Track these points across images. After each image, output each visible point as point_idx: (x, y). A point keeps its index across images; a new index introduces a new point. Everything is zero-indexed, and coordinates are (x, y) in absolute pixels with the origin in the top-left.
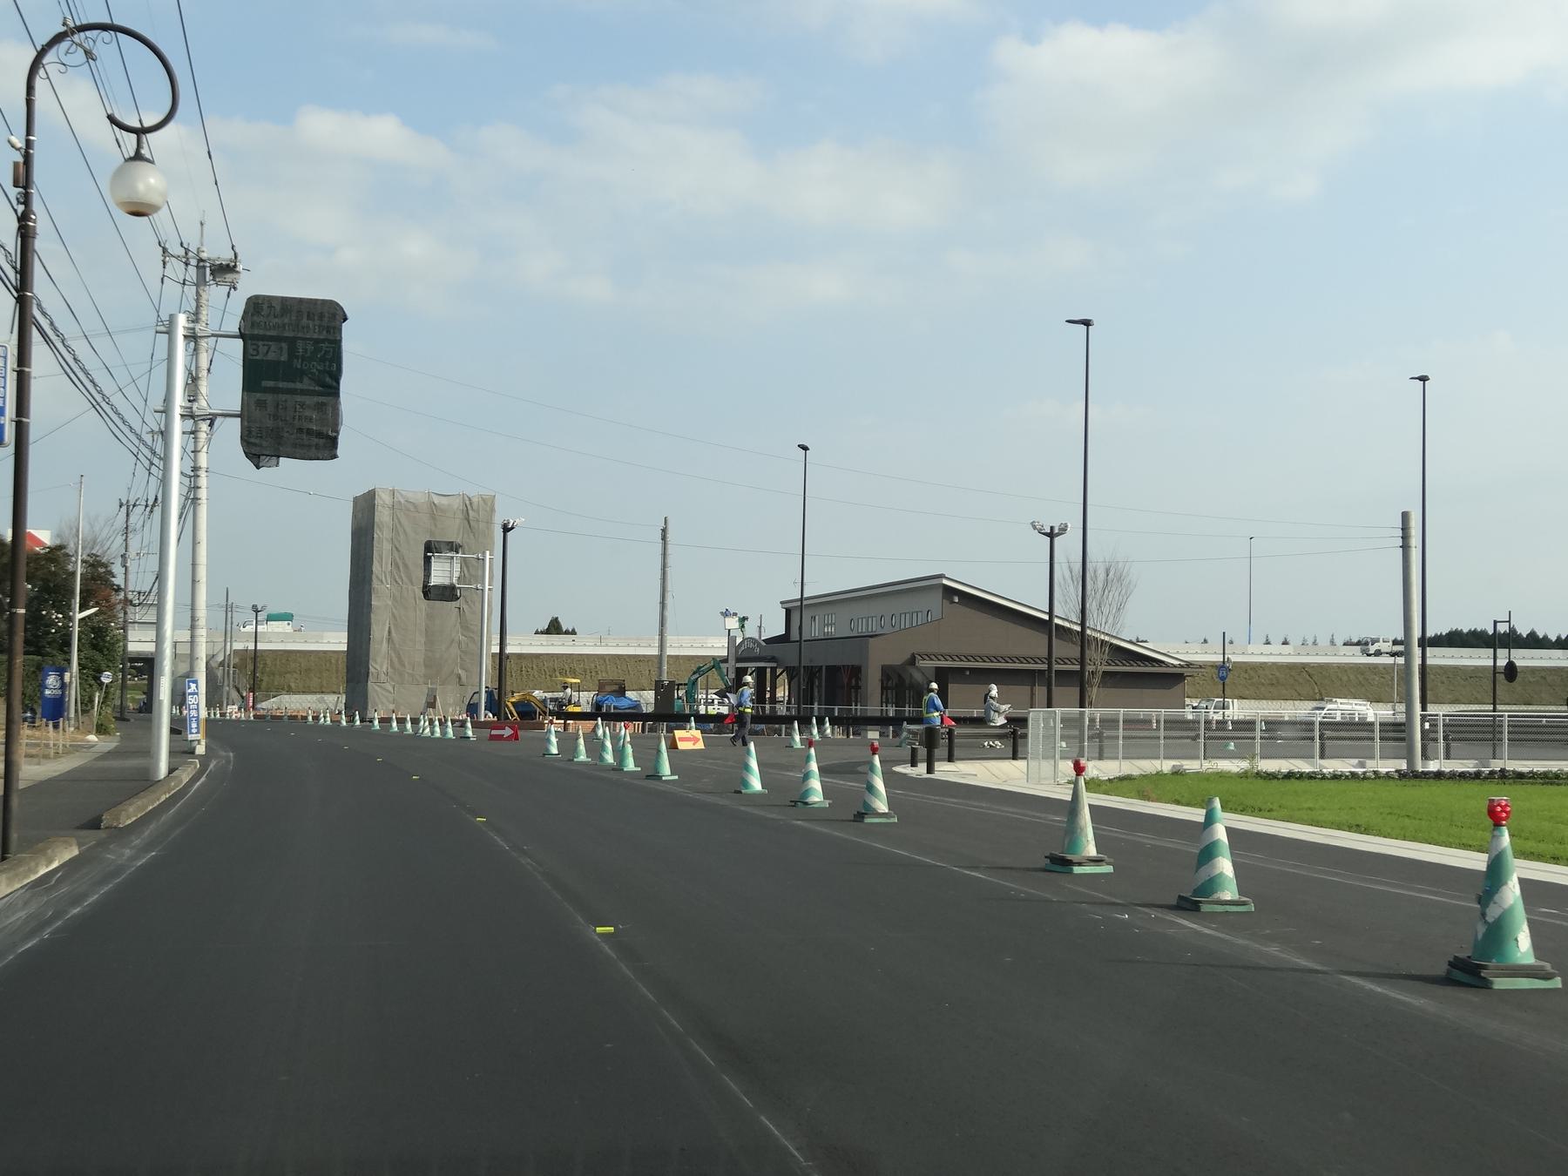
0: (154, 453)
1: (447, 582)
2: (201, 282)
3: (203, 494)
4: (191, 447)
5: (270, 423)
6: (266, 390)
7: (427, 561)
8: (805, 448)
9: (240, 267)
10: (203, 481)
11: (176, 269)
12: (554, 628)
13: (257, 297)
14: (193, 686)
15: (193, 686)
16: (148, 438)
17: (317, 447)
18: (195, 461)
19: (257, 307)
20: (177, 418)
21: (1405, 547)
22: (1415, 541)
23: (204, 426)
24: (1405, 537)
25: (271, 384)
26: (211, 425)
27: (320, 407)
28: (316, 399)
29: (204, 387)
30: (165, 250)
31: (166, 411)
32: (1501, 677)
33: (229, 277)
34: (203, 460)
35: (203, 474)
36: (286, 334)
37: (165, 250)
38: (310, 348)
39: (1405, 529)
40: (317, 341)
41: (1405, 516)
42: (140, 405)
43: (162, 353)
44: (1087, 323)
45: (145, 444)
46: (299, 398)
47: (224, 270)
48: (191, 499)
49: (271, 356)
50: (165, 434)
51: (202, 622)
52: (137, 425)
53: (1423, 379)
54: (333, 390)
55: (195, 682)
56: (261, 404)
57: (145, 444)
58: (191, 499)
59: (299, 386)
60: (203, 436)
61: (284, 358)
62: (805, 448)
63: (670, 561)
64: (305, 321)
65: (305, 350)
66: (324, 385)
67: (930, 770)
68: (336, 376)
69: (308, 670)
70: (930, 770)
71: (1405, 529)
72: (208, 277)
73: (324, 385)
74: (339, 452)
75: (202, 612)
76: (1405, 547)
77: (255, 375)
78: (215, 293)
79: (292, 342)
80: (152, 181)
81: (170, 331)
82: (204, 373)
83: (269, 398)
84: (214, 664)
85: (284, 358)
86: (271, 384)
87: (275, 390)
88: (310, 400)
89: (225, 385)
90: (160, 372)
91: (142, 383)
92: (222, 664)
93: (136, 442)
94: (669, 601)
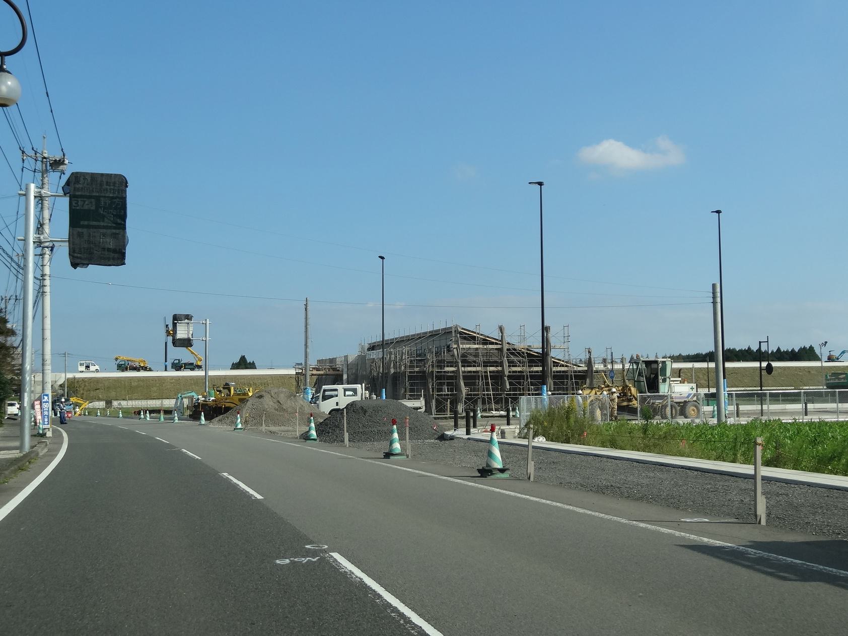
0: (19, 266)
1: (185, 336)
2: (44, 172)
3: (47, 289)
4: (40, 264)
5: (86, 246)
6: (83, 227)
7: (175, 325)
8: (382, 258)
9: (66, 162)
10: (47, 282)
11: (30, 163)
12: (242, 364)
13: (77, 173)
14: (46, 398)
15: (46, 398)
16: (16, 259)
17: (113, 259)
18: (42, 271)
19: (75, 178)
20: (31, 246)
21: (714, 303)
22: (719, 300)
23: (47, 251)
24: (714, 297)
25: (86, 223)
26: (52, 250)
27: (115, 236)
28: (114, 231)
29: (47, 228)
30: (23, 152)
31: (25, 240)
32: (764, 373)
33: (61, 167)
34: (47, 270)
35: (47, 278)
36: (94, 194)
37: (23, 152)
38: (108, 202)
39: (714, 293)
40: (113, 198)
41: (714, 286)
42: (11, 240)
43: (22, 211)
44: (540, 184)
45: (14, 262)
46: (102, 231)
47: (57, 164)
48: (40, 293)
49: (86, 207)
50: (25, 256)
51: (48, 362)
52: (9, 251)
53: (718, 212)
54: (123, 227)
55: (47, 395)
56: (80, 235)
57: (14, 262)
58: (40, 293)
59: (102, 224)
60: (47, 257)
61: (93, 208)
62: (382, 258)
63: (309, 321)
64: (105, 187)
65: (105, 203)
66: (116, 223)
67: (468, 433)
68: (124, 217)
69: (108, 388)
70: (468, 433)
71: (714, 293)
72: (49, 168)
73: (116, 223)
74: (126, 261)
75: (48, 356)
76: (714, 303)
77: (76, 218)
78: (53, 176)
79: (98, 199)
80: (9, 83)
81: (26, 195)
82: (47, 221)
83: (85, 231)
84: (57, 387)
85: (93, 208)
86: (86, 223)
87: (88, 227)
88: (109, 231)
89: (59, 226)
90: (21, 221)
91: (12, 228)
92: (61, 386)
93: (9, 260)
94: (309, 344)
